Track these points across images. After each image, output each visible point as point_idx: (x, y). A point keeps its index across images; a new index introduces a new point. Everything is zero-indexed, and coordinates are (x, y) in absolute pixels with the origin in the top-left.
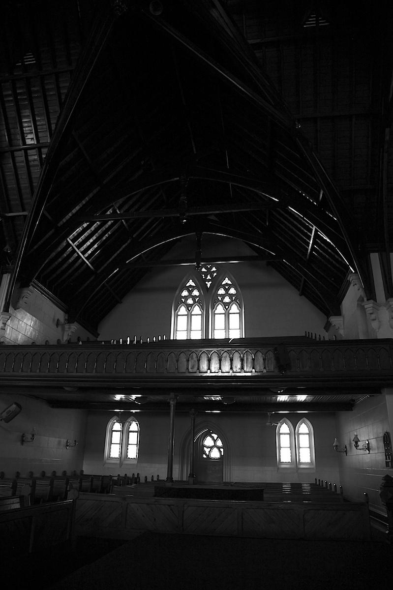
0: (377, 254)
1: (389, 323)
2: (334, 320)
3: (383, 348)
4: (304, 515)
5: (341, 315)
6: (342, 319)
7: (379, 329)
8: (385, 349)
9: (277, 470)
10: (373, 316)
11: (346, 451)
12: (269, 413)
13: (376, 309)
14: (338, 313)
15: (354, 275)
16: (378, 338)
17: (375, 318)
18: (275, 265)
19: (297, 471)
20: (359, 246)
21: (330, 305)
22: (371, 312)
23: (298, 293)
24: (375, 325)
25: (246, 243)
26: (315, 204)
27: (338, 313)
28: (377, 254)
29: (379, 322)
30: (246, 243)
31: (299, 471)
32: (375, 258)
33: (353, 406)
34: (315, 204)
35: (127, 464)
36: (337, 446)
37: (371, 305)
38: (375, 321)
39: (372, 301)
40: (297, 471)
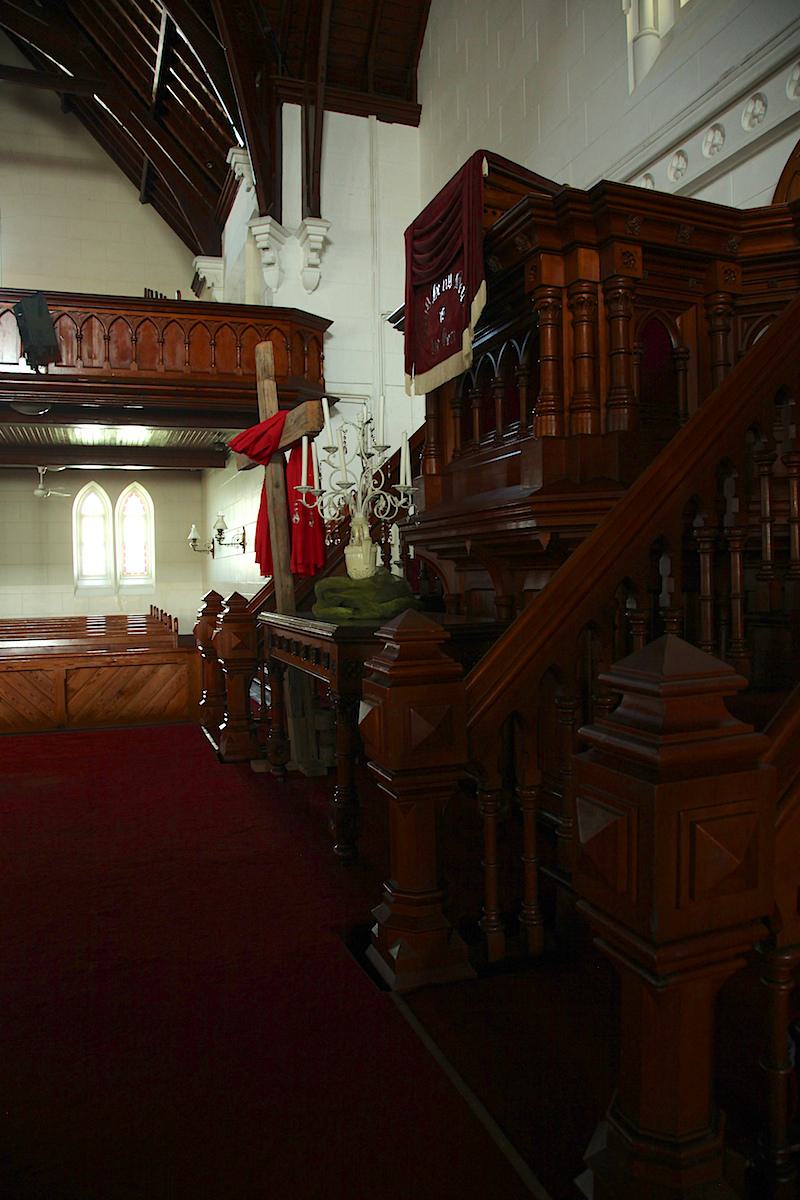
0: (299, 107)
1: (300, 277)
2: (206, 265)
3: (276, 328)
4: (66, 681)
5: (221, 256)
6: (222, 265)
7: (278, 287)
8: (279, 329)
9: (73, 589)
10: (268, 256)
11: (213, 551)
12: (40, 469)
13: (277, 240)
14: (216, 250)
15: (241, 151)
16: (274, 305)
17: (270, 260)
18: (76, 112)
19: (117, 592)
20: (258, 78)
21: (201, 231)
22: (265, 245)
23: (138, 193)
24: (270, 275)
25: (7, 32)
26: (787, 958)
27: (216, 250)
28: (298, 108)
29: (281, 270)
30: (7, 32)
31: (122, 591)
32: (292, 116)
33: (226, 459)
34: (787, 958)
35: (129, 587)
36: (195, 540)
37: (267, 228)
38: (271, 268)
39: (269, 219)
40: (117, 592)
